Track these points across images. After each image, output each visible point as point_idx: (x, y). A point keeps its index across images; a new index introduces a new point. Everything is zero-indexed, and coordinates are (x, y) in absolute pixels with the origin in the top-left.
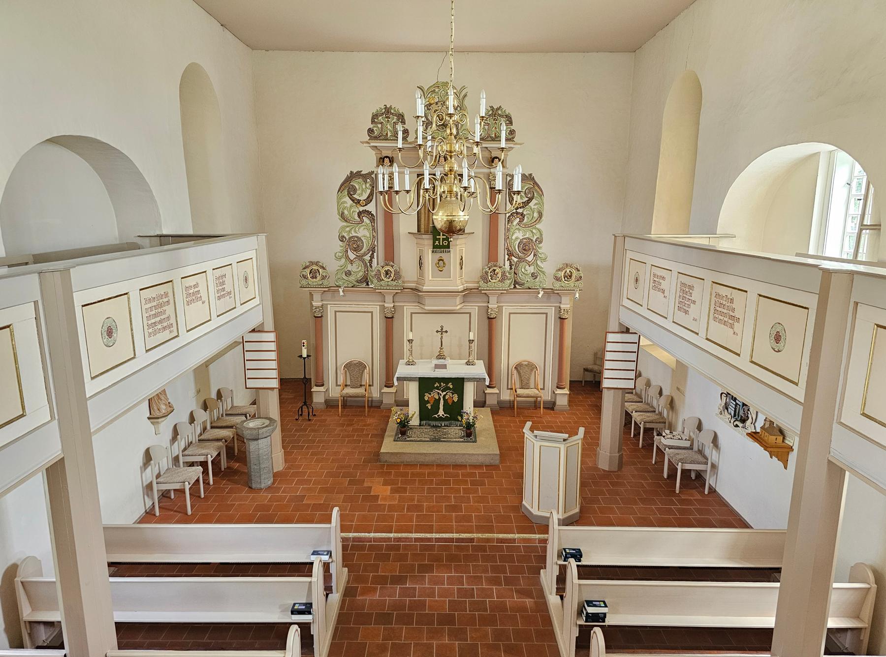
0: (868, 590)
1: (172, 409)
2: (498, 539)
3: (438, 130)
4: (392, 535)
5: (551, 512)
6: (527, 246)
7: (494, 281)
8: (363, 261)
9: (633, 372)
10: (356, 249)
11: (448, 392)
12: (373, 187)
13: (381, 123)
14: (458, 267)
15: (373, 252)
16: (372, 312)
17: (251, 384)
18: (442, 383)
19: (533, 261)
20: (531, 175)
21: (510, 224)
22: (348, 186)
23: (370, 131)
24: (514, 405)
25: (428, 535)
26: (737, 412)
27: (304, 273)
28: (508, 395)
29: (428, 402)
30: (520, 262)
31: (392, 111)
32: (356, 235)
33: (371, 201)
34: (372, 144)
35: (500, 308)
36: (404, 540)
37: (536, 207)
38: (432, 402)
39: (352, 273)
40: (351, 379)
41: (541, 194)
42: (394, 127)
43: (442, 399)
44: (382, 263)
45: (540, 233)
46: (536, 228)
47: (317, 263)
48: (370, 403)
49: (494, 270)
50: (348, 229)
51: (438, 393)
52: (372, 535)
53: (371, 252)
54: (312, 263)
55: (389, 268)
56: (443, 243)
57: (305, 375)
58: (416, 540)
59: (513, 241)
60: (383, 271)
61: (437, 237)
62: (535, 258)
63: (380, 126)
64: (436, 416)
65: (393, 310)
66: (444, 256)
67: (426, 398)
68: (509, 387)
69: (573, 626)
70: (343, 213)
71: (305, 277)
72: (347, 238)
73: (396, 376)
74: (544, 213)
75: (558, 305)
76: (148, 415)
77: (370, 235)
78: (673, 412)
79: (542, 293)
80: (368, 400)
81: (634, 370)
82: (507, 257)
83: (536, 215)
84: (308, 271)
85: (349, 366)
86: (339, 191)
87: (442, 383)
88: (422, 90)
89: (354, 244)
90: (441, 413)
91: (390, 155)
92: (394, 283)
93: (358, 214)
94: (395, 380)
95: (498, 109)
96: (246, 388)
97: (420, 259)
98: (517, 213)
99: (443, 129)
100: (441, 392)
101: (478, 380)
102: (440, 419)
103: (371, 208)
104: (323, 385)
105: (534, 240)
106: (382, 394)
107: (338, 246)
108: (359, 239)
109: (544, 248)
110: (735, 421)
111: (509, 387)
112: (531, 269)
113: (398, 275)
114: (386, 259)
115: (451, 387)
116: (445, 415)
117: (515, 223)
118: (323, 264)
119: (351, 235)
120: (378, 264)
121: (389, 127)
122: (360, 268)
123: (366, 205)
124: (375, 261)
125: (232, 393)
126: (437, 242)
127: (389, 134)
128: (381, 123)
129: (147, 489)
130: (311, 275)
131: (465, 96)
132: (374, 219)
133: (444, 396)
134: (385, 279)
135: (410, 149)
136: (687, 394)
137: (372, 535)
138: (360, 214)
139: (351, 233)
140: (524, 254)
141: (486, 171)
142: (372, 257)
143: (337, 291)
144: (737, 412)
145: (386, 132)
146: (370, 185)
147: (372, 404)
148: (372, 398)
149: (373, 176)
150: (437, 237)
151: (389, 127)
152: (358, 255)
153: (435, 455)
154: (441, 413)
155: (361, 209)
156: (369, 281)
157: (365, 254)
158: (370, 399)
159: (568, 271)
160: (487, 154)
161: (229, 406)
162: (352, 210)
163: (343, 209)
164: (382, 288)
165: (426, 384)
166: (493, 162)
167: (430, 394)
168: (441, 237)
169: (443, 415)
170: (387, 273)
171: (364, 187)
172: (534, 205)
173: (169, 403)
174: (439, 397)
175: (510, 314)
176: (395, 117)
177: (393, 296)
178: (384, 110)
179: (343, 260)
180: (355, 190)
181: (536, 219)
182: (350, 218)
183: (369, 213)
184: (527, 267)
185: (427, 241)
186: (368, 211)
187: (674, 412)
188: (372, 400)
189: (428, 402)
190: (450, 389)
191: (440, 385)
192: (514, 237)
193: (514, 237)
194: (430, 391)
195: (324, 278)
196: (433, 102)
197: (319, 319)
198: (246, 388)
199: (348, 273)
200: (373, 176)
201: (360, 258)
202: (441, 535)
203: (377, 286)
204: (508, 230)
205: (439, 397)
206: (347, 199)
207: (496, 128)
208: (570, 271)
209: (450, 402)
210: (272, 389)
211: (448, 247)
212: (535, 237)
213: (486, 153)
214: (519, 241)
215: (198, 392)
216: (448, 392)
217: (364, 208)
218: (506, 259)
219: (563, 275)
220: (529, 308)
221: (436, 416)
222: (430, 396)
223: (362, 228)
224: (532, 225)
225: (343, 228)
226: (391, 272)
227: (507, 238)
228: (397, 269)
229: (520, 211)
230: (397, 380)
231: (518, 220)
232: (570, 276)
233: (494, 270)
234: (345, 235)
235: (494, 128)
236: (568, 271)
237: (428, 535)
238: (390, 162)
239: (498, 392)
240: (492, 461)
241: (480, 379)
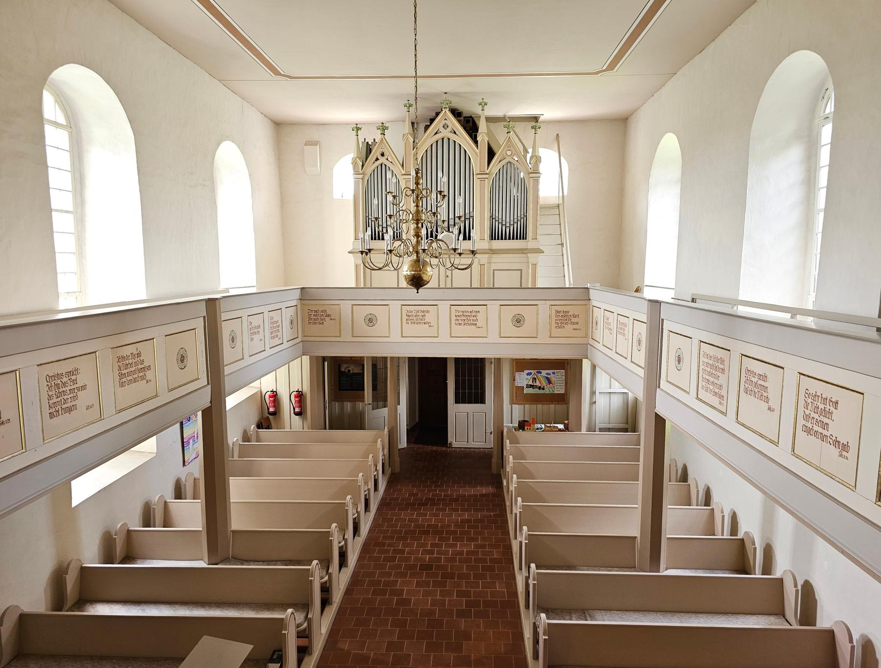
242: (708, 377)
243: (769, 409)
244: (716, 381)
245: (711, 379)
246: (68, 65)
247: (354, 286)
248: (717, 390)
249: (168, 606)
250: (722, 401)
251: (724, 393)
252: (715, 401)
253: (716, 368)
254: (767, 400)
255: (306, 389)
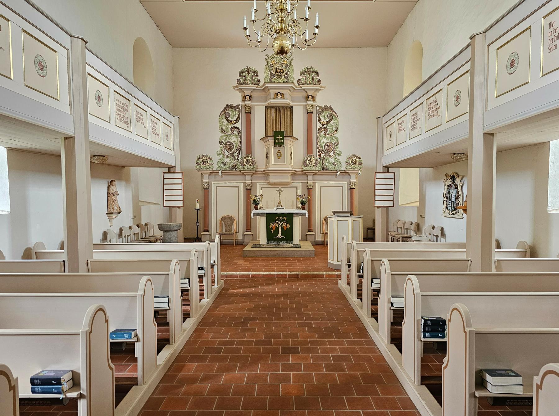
0: (526, 253)
1: (120, 211)
2: (313, 275)
3: (277, 78)
4: (250, 273)
5: (343, 237)
6: (329, 146)
7: (311, 165)
8: (233, 156)
9: (392, 202)
10: (229, 150)
11: (284, 222)
12: (240, 113)
13: (244, 76)
14: (289, 158)
15: (240, 151)
16: (238, 187)
17: (167, 204)
18: (280, 217)
19: (333, 155)
20: (330, 106)
21: (319, 134)
22: (225, 113)
23: (238, 81)
24: (324, 243)
25: (272, 273)
26: (452, 206)
27: (199, 162)
28: (321, 238)
29: (272, 229)
30: (326, 156)
31: (251, 70)
32: (230, 141)
33: (238, 121)
34: (239, 88)
35: (315, 183)
36: (257, 276)
37: (334, 124)
38: (274, 229)
39: (227, 163)
40: (225, 227)
41: (337, 118)
42: (252, 78)
43: (280, 227)
44: (244, 155)
45: (337, 139)
46: (334, 136)
47: (206, 156)
48: (236, 243)
49: (311, 159)
50: (225, 137)
51: (278, 223)
52: (238, 273)
53: (238, 151)
54: (203, 156)
55: (249, 158)
56: (280, 141)
57: (197, 236)
58: (265, 276)
59: (321, 144)
60: (245, 160)
61: (277, 138)
62: (334, 154)
63: (244, 78)
64: (277, 237)
65: (251, 184)
66: (281, 149)
67: (271, 227)
68: (321, 232)
69: (355, 277)
70: (222, 128)
71: (199, 164)
72: (224, 143)
73: (253, 212)
74: (339, 128)
75: (349, 181)
76: (107, 212)
77: (238, 141)
78: (419, 232)
79: (339, 172)
80: (235, 241)
81: (392, 201)
82: (318, 154)
83: (334, 129)
84: (201, 160)
85: (223, 219)
86: (220, 115)
87: (280, 217)
88: (268, 57)
89: (228, 146)
90: (280, 235)
91: (250, 95)
92: (252, 167)
93: (231, 128)
94: (252, 215)
95: (311, 68)
96: (164, 207)
97: (267, 153)
98: (323, 128)
99: (280, 77)
100: (279, 223)
101: (302, 215)
102: (279, 240)
103: (238, 125)
104: (208, 231)
105: (334, 143)
106: (244, 236)
107: (218, 147)
108: (231, 143)
109: (340, 148)
110: (452, 212)
111: (321, 232)
112: (332, 160)
113: (254, 163)
114: (247, 153)
115: (286, 219)
116: (282, 237)
117: (322, 133)
118: (210, 156)
119: (227, 141)
120: (242, 156)
121: (249, 78)
122: (231, 160)
123: (235, 123)
124: (240, 156)
125: (154, 227)
126: (277, 140)
127: (249, 82)
128: (244, 76)
129: (103, 240)
130: (203, 163)
131: (292, 59)
132: (240, 132)
133: (282, 225)
134: (246, 165)
135: (261, 91)
136: (426, 217)
137: (238, 273)
138: (232, 129)
139: (227, 140)
140: (328, 151)
141: (305, 103)
142: (239, 154)
143: (218, 173)
144: (452, 206)
145: (247, 81)
146: (238, 112)
147: (238, 243)
148: (238, 240)
149: (240, 107)
150: (277, 138)
151: (249, 78)
152: (230, 152)
153: (276, 251)
154: (280, 235)
155: (233, 126)
156: (237, 168)
157: (234, 152)
158: (236, 241)
159: (354, 159)
160: (305, 94)
161: (152, 235)
162: (227, 126)
163: (222, 126)
164: (244, 170)
165: (270, 218)
166: (308, 98)
167: (273, 224)
168: (279, 138)
169: (281, 237)
170: (247, 161)
171: (234, 113)
172: (333, 123)
173: (119, 207)
174: (278, 225)
175: (321, 187)
176: (253, 73)
177: (251, 176)
178: (246, 69)
179: (222, 156)
180: (229, 115)
181: (334, 131)
182: (226, 131)
183: (237, 128)
184: (330, 159)
185: (271, 141)
186: (237, 127)
187: (420, 231)
188: (238, 241)
189: (272, 229)
190: (285, 220)
191: (279, 218)
192: (322, 142)
193: (322, 142)
194: (273, 222)
195: (210, 164)
196: (274, 63)
197: (207, 190)
198: (164, 207)
199: (225, 164)
200: (240, 107)
201: (232, 154)
202: (279, 272)
203: (241, 169)
204: (318, 137)
205: (278, 225)
206: (225, 120)
207: (309, 78)
208: (355, 159)
209: (285, 229)
210: (179, 207)
211: (283, 143)
212: (334, 142)
213: (304, 94)
214: (325, 144)
215: (135, 217)
216: (284, 222)
217: (234, 125)
218: (318, 155)
219: (351, 161)
220: (332, 183)
221: (277, 237)
222: (273, 225)
223: (233, 137)
224: (332, 134)
225: (222, 137)
226: (250, 160)
227: (317, 142)
228: (254, 158)
229: (325, 126)
230: (253, 215)
231: (324, 131)
232: (356, 162)
233: (311, 159)
234: (223, 141)
235: (308, 79)
236: (354, 159)
237: (272, 273)
238: (249, 98)
239: (314, 234)
240: (310, 255)
241: (303, 214)
242: (120, 113)
243: (144, 127)
244: (124, 116)
245: (122, 114)
246: (308, 222)
247: (180, 171)
248: (125, 121)
249: (480, 391)
250: (128, 126)
251: (129, 122)
252: (125, 126)
253: (125, 109)
254: (143, 123)
255: (66, 260)
